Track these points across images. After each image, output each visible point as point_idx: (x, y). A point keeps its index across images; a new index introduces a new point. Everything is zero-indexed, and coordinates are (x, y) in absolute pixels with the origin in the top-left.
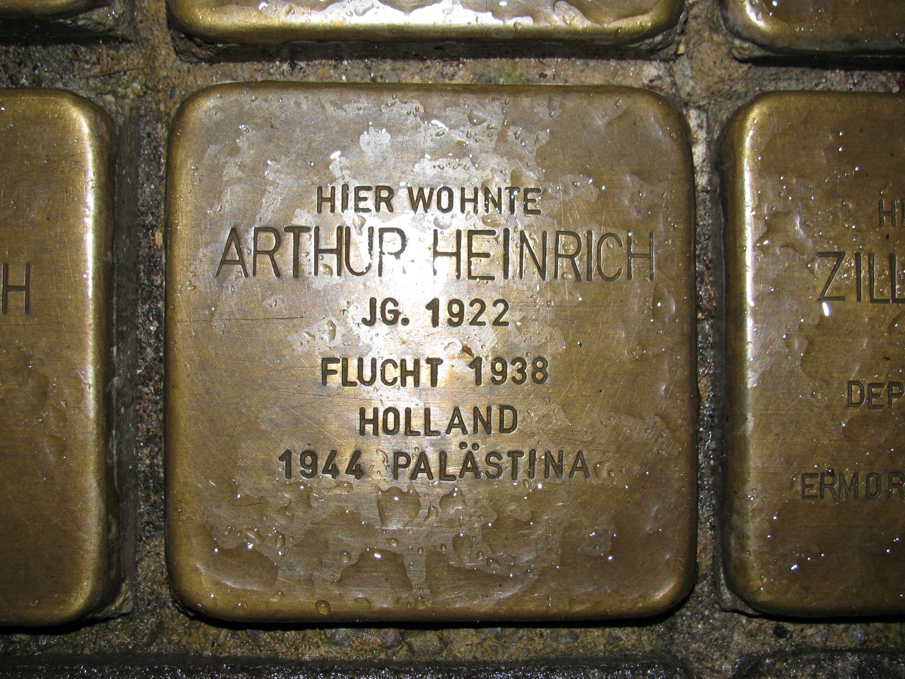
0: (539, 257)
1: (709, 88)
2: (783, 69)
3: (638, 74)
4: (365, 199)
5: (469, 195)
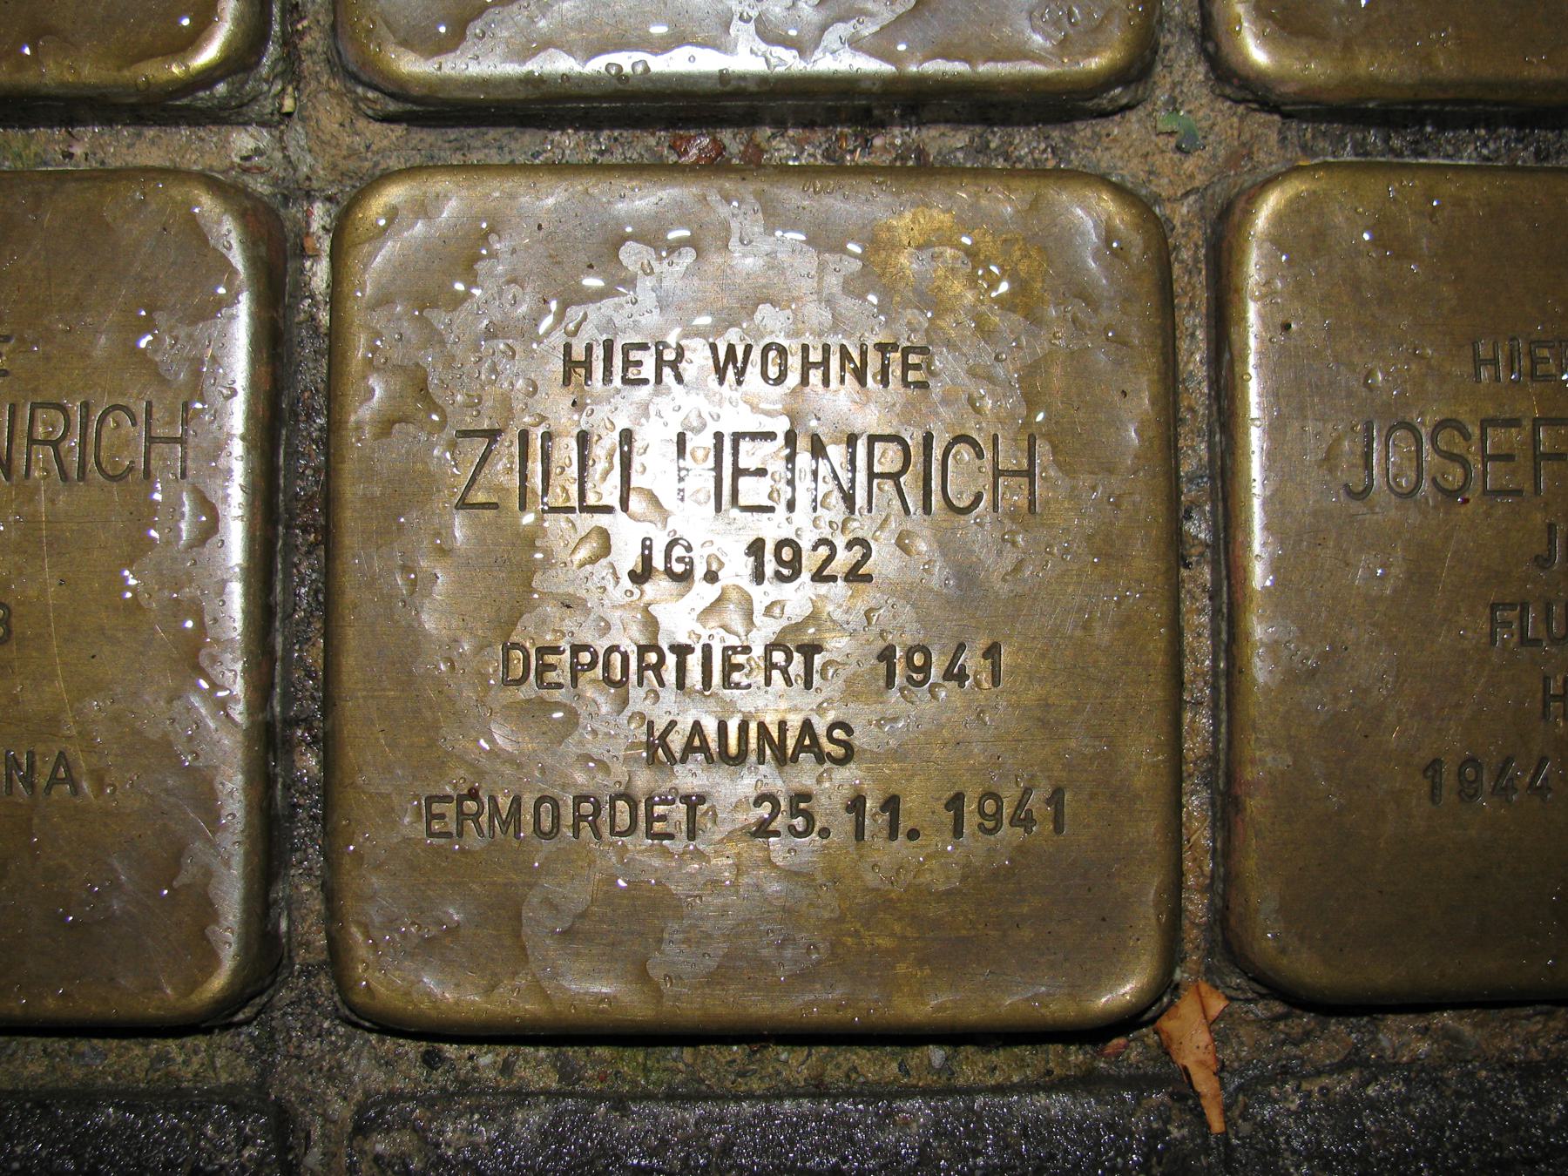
0: (845, 477)
1: (334, 166)
2: (472, 131)
3: (224, 144)
4: (553, 667)
5: (816, 356)
